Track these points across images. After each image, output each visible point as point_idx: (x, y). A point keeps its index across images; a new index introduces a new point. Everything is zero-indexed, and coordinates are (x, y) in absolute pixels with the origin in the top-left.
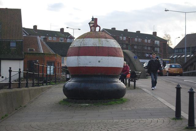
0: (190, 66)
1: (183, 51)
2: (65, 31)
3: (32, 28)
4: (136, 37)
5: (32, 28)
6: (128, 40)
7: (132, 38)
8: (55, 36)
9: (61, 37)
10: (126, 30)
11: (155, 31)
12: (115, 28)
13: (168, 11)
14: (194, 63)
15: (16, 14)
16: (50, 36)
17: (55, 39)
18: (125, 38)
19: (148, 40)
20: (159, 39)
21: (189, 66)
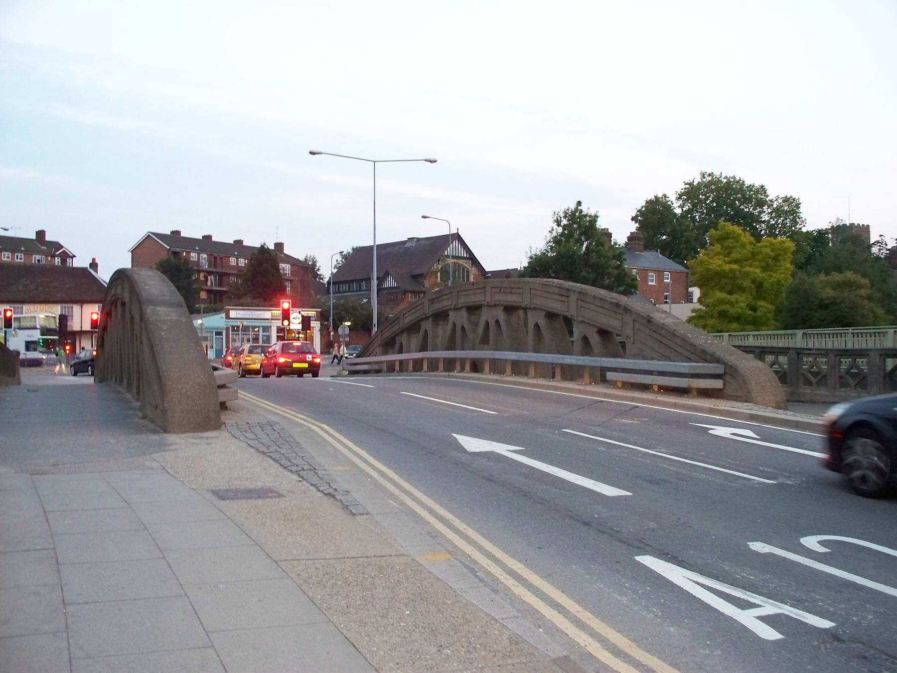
0: (405, 335)
1: (339, 289)
2: (47, 239)
3: (33, 236)
4: (233, 255)
5: (33, 236)
6: (214, 261)
7: (221, 255)
8: (20, 251)
9: (38, 253)
10: (208, 238)
11: (279, 241)
12: (178, 233)
13: (429, 217)
14: (422, 323)
15: (517, 269)
16: (6, 250)
17: (20, 258)
18: (205, 256)
19: (237, 259)
20: (290, 259)
21: (402, 332)
